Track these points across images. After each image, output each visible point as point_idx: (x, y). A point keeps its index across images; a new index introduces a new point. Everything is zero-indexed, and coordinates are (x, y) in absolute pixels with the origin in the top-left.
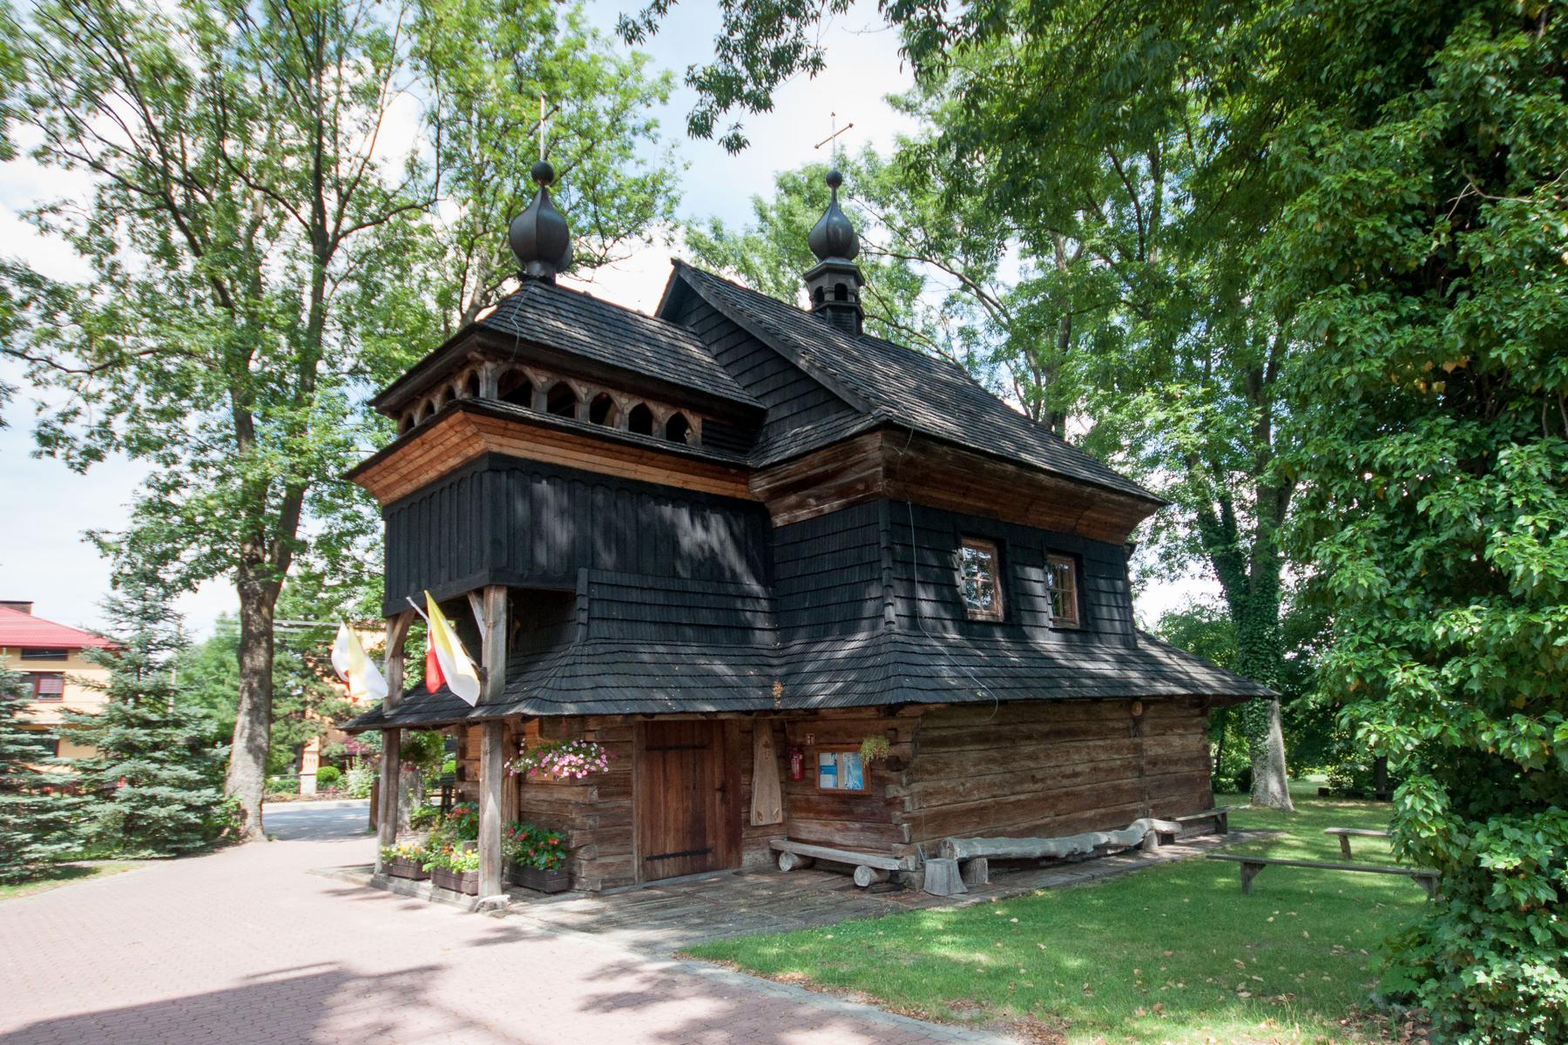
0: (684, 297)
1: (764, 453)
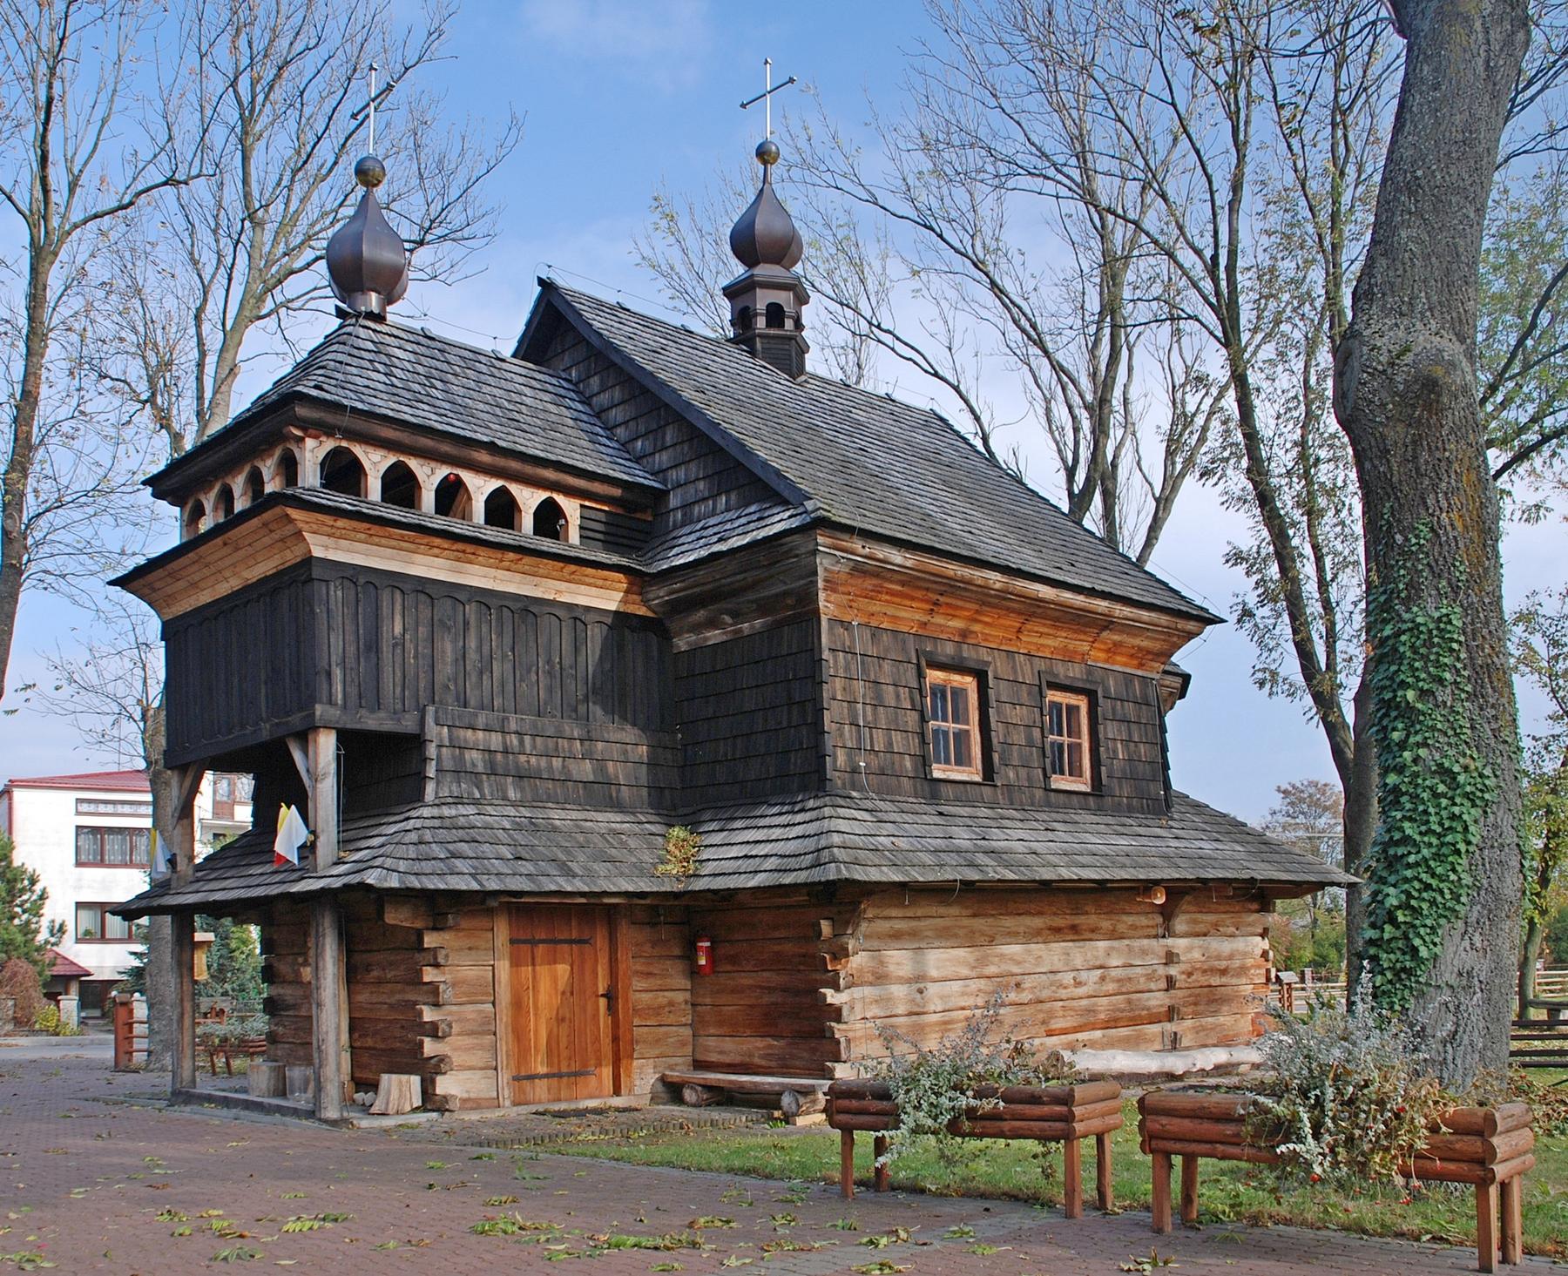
0: (557, 330)
1: (653, 560)
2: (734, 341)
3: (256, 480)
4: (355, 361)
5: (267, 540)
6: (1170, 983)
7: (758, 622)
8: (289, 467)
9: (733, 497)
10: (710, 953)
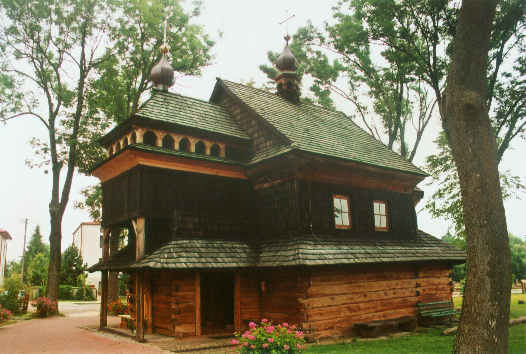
0: (222, 93)
2: (276, 94)
3: (126, 141)
4: (157, 105)
5: (127, 159)
6: (418, 293)
7: (279, 181)
8: (134, 137)
9: (271, 141)
10: (266, 286)
